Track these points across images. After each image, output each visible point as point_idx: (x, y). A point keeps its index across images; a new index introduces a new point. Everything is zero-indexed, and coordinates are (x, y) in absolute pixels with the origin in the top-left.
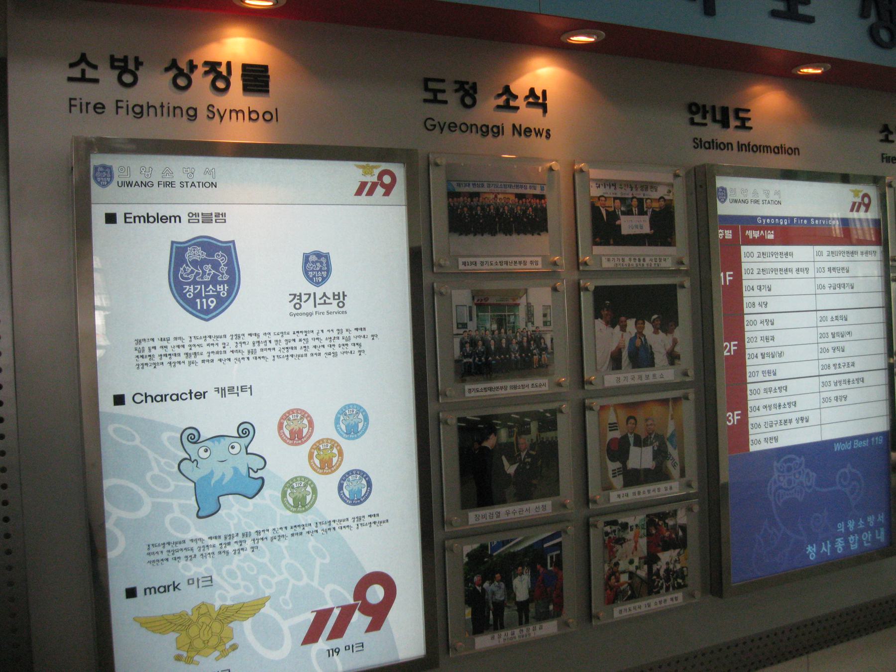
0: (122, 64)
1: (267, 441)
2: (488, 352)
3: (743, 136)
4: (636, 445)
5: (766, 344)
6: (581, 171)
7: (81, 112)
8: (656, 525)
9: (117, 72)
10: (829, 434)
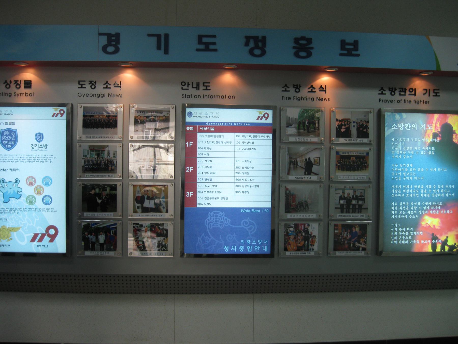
1: (23, 184)
2: (93, 164)
3: (207, 93)
4: (147, 199)
5: (207, 169)
6: (333, 111)
8: (155, 228)
10: (238, 205)
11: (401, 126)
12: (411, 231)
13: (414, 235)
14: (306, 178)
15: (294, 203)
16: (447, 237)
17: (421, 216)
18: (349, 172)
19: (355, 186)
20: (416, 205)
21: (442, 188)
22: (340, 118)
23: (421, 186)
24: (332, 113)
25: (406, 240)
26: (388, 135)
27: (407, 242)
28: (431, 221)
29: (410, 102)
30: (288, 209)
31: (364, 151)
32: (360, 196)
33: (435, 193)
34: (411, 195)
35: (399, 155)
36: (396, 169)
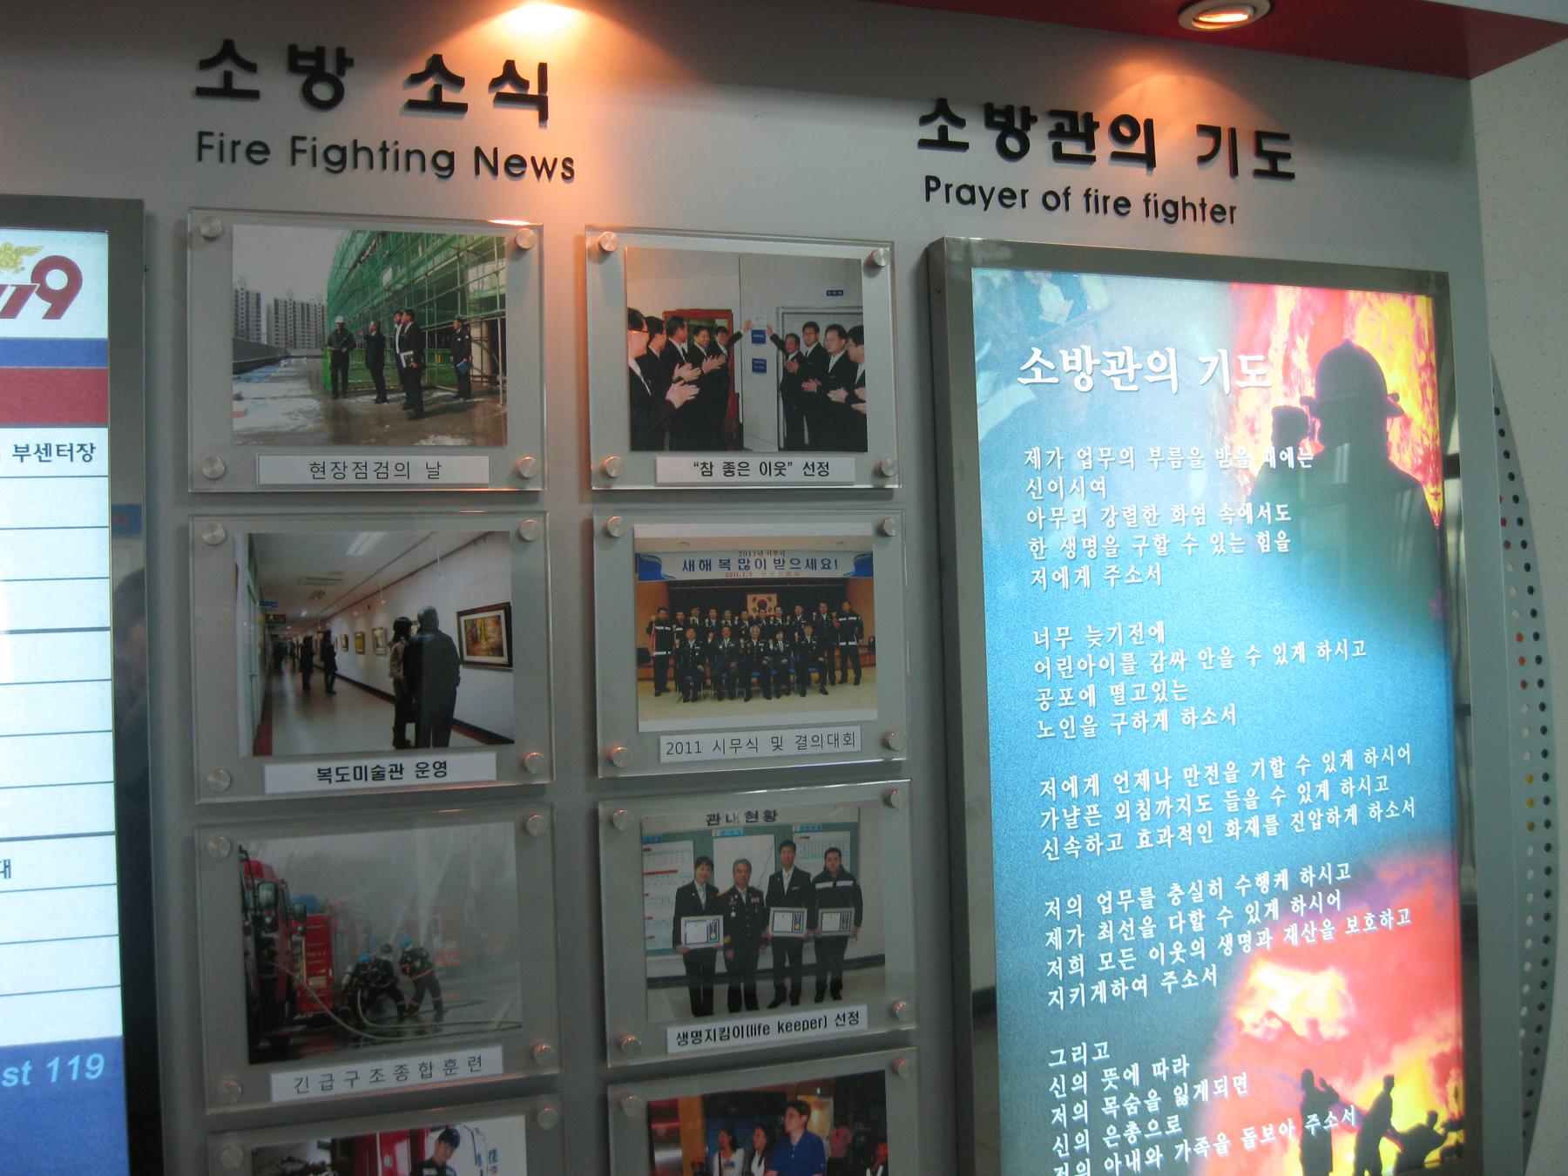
0: (311, 63)
6: (604, 254)
7: (222, 160)
9: (996, 134)
11: (1077, 360)
12: (1174, 1080)
13: (1195, 1104)
14: (413, 771)
15: (320, 982)
16: (1389, 1083)
17: (1233, 969)
18: (739, 704)
19: (791, 804)
20: (1198, 898)
21: (1343, 773)
22: (653, 308)
23: (1222, 768)
24: (593, 269)
25: (1151, 1143)
26: (997, 431)
27: (1155, 1157)
28: (1294, 998)
29: (1122, 205)
30: (281, 1023)
31: (841, 541)
32: (821, 878)
33: (1307, 808)
34: (1166, 836)
35: (1073, 563)
36: (1064, 664)
